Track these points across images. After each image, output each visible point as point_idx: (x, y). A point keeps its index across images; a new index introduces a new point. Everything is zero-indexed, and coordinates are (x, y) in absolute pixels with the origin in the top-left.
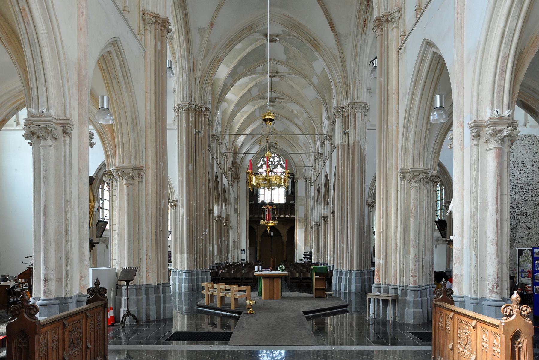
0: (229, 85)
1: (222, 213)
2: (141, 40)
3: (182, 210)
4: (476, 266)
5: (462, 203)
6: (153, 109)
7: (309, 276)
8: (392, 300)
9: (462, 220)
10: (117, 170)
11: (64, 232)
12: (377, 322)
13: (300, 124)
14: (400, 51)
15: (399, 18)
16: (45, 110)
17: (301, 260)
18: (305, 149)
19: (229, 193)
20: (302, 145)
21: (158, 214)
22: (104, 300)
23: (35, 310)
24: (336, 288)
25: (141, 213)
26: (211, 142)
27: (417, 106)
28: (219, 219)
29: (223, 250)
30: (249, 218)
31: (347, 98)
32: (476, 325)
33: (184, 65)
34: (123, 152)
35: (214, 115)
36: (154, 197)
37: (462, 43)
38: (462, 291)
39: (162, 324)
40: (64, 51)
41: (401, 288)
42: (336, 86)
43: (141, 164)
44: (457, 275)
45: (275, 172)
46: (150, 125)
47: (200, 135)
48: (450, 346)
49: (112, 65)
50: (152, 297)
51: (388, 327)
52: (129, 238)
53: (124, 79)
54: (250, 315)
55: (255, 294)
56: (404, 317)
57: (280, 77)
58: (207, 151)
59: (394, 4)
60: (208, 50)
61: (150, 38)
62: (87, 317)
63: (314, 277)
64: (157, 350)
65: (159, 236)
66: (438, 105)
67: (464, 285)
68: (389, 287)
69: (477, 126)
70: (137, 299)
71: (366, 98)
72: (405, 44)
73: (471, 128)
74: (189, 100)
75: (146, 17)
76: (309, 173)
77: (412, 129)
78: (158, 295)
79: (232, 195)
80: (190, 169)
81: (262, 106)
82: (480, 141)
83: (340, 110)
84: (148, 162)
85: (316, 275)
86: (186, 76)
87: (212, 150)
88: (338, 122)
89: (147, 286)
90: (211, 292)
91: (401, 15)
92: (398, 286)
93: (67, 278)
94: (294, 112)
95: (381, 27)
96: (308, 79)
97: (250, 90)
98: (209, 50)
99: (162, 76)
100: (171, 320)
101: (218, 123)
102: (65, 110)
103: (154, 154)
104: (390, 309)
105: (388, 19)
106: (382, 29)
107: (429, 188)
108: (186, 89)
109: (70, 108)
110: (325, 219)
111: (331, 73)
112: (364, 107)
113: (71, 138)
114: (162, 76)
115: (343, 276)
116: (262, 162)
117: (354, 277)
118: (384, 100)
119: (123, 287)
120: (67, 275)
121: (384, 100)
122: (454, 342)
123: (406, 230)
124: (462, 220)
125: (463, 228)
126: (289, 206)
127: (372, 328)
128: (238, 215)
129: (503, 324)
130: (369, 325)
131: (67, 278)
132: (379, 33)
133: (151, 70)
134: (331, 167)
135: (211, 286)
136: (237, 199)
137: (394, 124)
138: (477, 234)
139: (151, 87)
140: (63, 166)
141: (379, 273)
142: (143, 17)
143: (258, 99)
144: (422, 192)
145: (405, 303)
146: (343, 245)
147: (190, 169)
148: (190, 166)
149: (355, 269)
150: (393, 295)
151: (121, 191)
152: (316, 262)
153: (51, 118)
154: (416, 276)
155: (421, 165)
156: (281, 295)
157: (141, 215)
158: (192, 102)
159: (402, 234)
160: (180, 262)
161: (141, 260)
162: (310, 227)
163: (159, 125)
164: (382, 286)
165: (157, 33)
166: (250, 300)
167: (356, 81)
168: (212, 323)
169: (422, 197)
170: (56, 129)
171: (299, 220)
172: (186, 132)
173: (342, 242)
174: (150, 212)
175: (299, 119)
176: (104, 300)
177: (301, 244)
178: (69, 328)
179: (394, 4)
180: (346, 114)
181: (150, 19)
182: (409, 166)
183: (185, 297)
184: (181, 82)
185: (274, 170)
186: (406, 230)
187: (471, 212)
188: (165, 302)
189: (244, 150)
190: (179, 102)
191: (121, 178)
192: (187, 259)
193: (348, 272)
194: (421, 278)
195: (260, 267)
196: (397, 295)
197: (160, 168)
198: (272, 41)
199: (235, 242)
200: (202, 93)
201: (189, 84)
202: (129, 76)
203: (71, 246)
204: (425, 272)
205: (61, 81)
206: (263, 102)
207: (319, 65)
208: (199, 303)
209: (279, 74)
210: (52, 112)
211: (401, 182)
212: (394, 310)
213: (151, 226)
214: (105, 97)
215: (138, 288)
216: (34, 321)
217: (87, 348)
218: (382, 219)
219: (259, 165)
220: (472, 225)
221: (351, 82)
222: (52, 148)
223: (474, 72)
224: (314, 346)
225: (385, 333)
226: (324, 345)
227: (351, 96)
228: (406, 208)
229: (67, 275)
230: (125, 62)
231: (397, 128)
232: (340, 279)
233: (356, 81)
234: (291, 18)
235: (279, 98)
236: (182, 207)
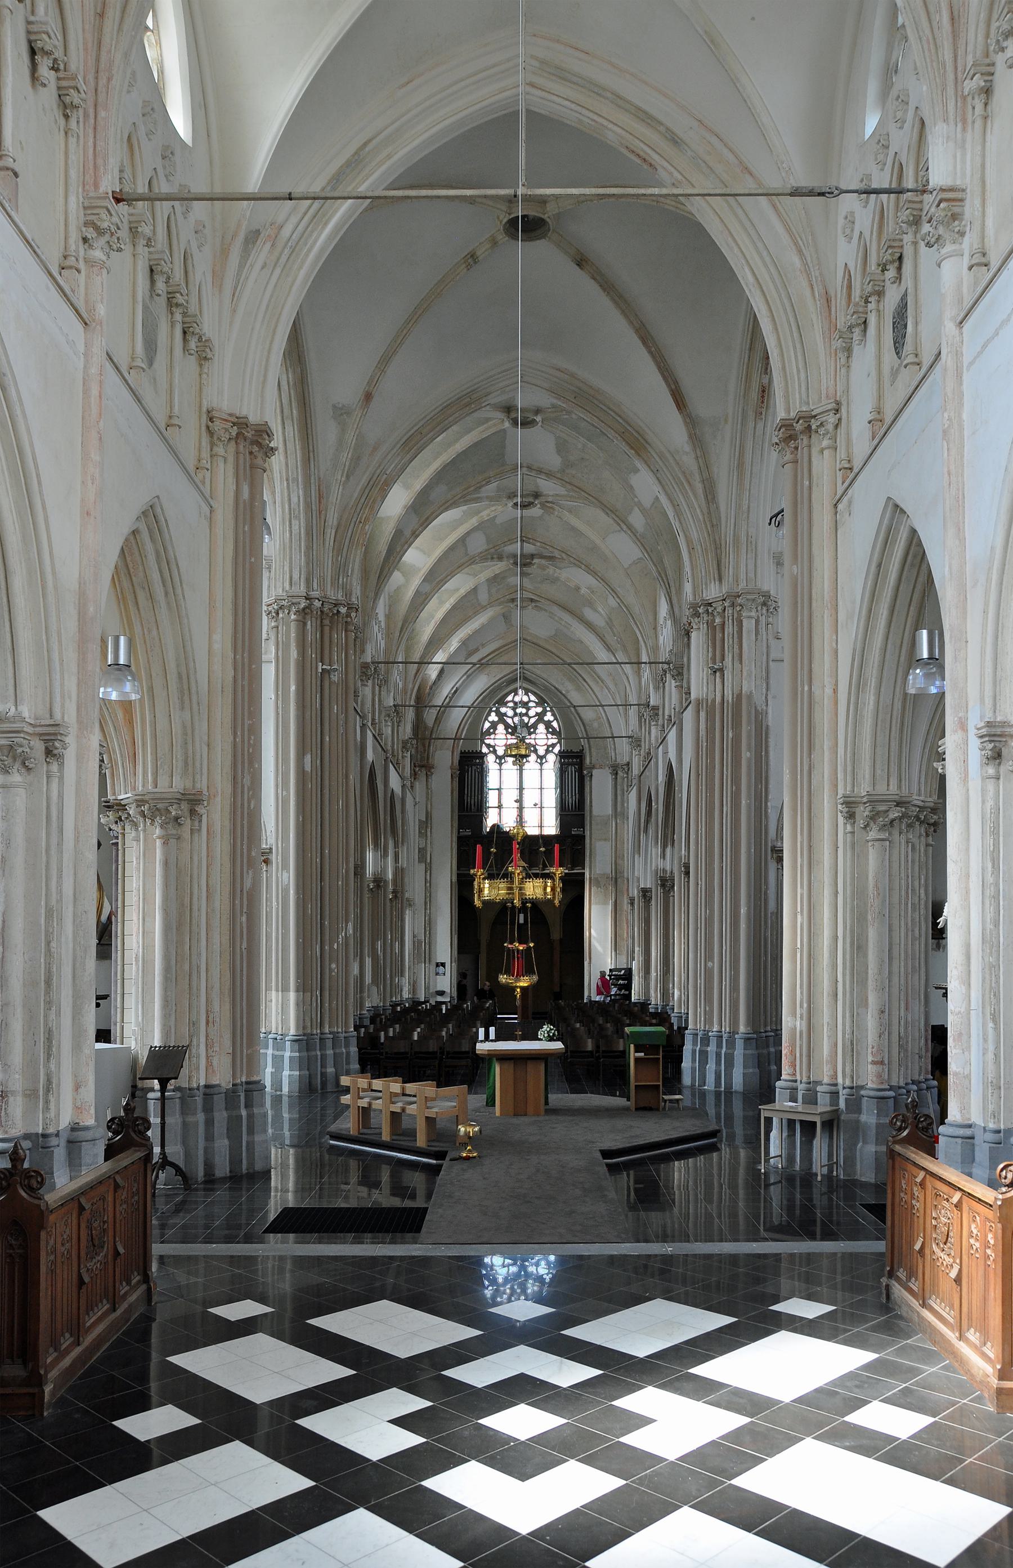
0: (407, 533)
1: (384, 869)
2: (204, 483)
3: (285, 875)
4: (996, 1056)
5: (967, 908)
6: (229, 645)
7: (621, 1049)
8: (823, 1124)
9: (968, 946)
10: (140, 803)
11: (43, 983)
12: (788, 1178)
13: (599, 622)
14: (840, 506)
15: (836, 426)
16: (13, 709)
19: (403, 811)
21: (238, 907)
22: (145, 1145)
23: (39, 1179)
24: (693, 1078)
25: (195, 907)
26: (359, 683)
27: (879, 645)
28: (378, 886)
29: (388, 969)
30: (458, 875)
31: (720, 580)
32: (960, 1201)
33: (294, 500)
34: (156, 760)
35: (369, 614)
36: (227, 865)
37: (962, 541)
38: (969, 1113)
39: (244, 1186)
40: (54, 573)
41: (845, 1091)
42: (691, 549)
43: (198, 785)
44: (956, 1074)
46: (219, 686)
47: (335, 678)
48: (917, 1247)
49: (138, 559)
50: (221, 1116)
51: (814, 1190)
52: (167, 970)
53: (164, 586)
54: (467, 1163)
55: (476, 1100)
56: (853, 1165)
57: (543, 506)
58: (352, 711)
59: (824, 392)
60: (356, 460)
61: (224, 477)
62: (117, 1187)
63: (633, 1055)
64: (232, 1257)
65: (238, 962)
66: (925, 655)
67: (972, 1096)
68: (819, 1088)
69: (994, 735)
70: (185, 1124)
71: (768, 581)
72: (850, 492)
73: (981, 737)
74: (308, 587)
75: (217, 426)
76: (623, 751)
77: (870, 699)
78: (234, 1113)
79: (412, 815)
80: (308, 768)
81: (496, 577)
82: (1002, 767)
83: (701, 610)
84: (217, 783)
85: (636, 1051)
86: (299, 526)
87: (363, 704)
88: (698, 639)
89: (208, 1091)
90: (367, 1100)
91: (840, 420)
92: (840, 1088)
93: (48, 1090)
94: (584, 591)
95: (792, 444)
96: (621, 520)
97: (463, 540)
98: (359, 458)
99: (251, 563)
100: (266, 1174)
101: (376, 628)
102: (51, 704)
103: (228, 762)
104: (819, 1145)
105: (809, 427)
106: (796, 448)
107: (916, 841)
108: (300, 559)
109: (63, 697)
110: (666, 883)
111: (678, 514)
112: (764, 604)
113: (61, 765)
114: (251, 563)
115: (712, 1048)
116: (493, 717)
117: (739, 1052)
118: (802, 621)
119: (150, 1095)
120: (49, 1081)
121: (802, 621)
122: (924, 1238)
123: (859, 948)
124: (968, 946)
125: (969, 966)
127: (775, 1192)
128: (429, 868)
129: (999, 1203)
130: (767, 1186)
131: (48, 1090)
132: (789, 457)
133: (225, 550)
134: (680, 749)
135: (366, 1086)
136: (426, 825)
137: (828, 681)
138: (998, 982)
139: (224, 593)
140: (44, 831)
141: (792, 1052)
142: (208, 427)
143: (486, 559)
144: (896, 852)
145: (856, 1130)
146: (710, 964)
147: (308, 768)
148: (308, 758)
149: (742, 1029)
150: (829, 1109)
151: (148, 854)
152: (642, 998)
153: (23, 724)
154: (882, 1063)
155: (893, 788)
156: (547, 1103)
157: (195, 914)
158: (315, 594)
159: (848, 957)
160: (280, 1012)
161: (193, 1024)
162: (626, 901)
163: (243, 686)
164: (801, 1087)
165: (241, 461)
166: (466, 1124)
167: (743, 539)
168: (369, 1181)
169: (896, 865)
170: (31, 748)
171: (596, 882)
172: (297, 673)
173: (709, 957)
174: (217, 904)
175: (596, 610)
176: (145, 1145)
177: (602, 948)
178: (86, 1215)
179: (824, 392)
180: (718, 620)
181: (226, 430)
182: (864, 789)
183: (290, 1106)
184: (287, 541)
186: (858, 947)
187: (984, 929)
188: (251, 1131)
190: (280, 592)
191: (149, 822)
192: (297, 1004)
193: (725, 1036)
194: (895, 1066)
195: (492, 1030)
196: (837, 1110)
197: (243, 792)
198: (527, 423)
199: (420, 942)
200: (341, 569)
201: (307, 548)
202: (176, 579)
203: (58, 1014)
204: (906, 1051)
205: (44, 637)
206: (498, 567)
207: (645, 484)
208: (333, 1128)
209: (542, 499)
210: (26, 712)
211: (845, 828)
212: (830, 1146)
213: (220, 938)
214: (122, 638)
215: (186, 1095)
216: (36, 1202)
217: (117, 1253)
218: (799, 916)
219: (487, 725)
220: (987, 959)
221: (730, 539)
222: (22, 792)
223: (985, 612)
224: (623, 1245)
225: (808, 1208)
226: (646, 1241)
227: (729, 573)
228: (858, 892)
229: (49, 1081)
230: (169, 548)
231: (835, 691)
232: (704, 1054)
233: (743, 539)
234: (573, 376)
235: (542, 557)
236: (285, 866)
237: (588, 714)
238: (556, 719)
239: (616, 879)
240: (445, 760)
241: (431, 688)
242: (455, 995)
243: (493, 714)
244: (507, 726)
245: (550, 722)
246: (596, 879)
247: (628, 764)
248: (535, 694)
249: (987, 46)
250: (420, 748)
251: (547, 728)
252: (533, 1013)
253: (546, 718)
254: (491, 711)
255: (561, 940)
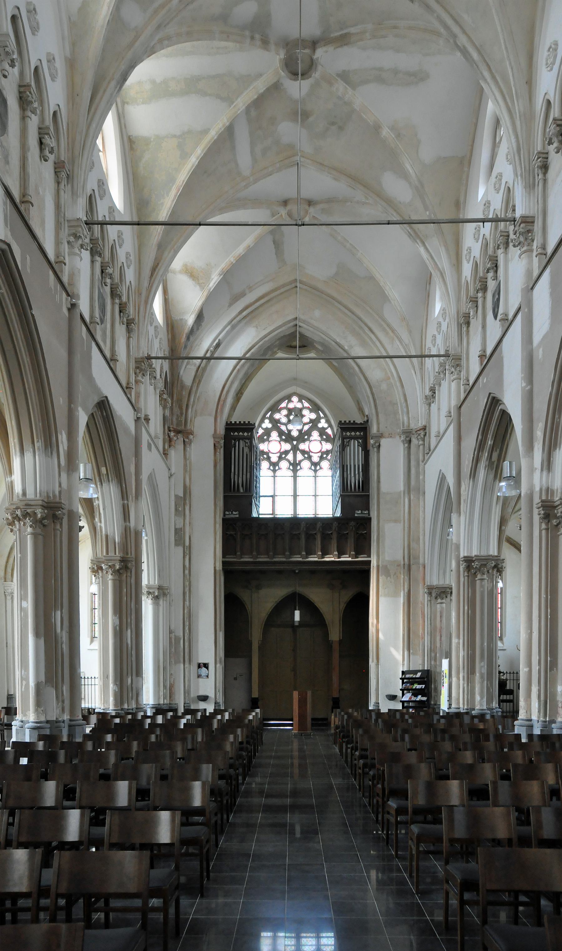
17: (392, 698)
18: (405, 336)
20: (395, 322)
30: (224, 563)
45: (303, 452)
89: (22, 89)
94: (385, 132)
116: (267, 424)
126: (353, 523)
128: (188, 552)
171: (384, 570)
185: (302, 446)
189: (204, 345)
199: (177, 639)
237: (374, 371)
238: (330, 426)
239: (409, 566)
240: (206, 430)
241: (188, 338)
242: (221, 700)
243: (267, 421)
244: (281, 433)
245: (324, 429)
246: (385, 567)
247: (424, 428)
248: (309, 400)
249: (496, 278)
250: (176, 410)
251: (321, 435)
252: (313, 719)
253: (320, 425)
254: (264, 418)
255: (340, 642)
